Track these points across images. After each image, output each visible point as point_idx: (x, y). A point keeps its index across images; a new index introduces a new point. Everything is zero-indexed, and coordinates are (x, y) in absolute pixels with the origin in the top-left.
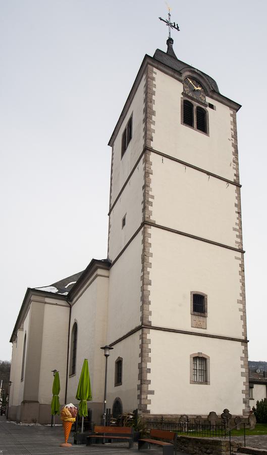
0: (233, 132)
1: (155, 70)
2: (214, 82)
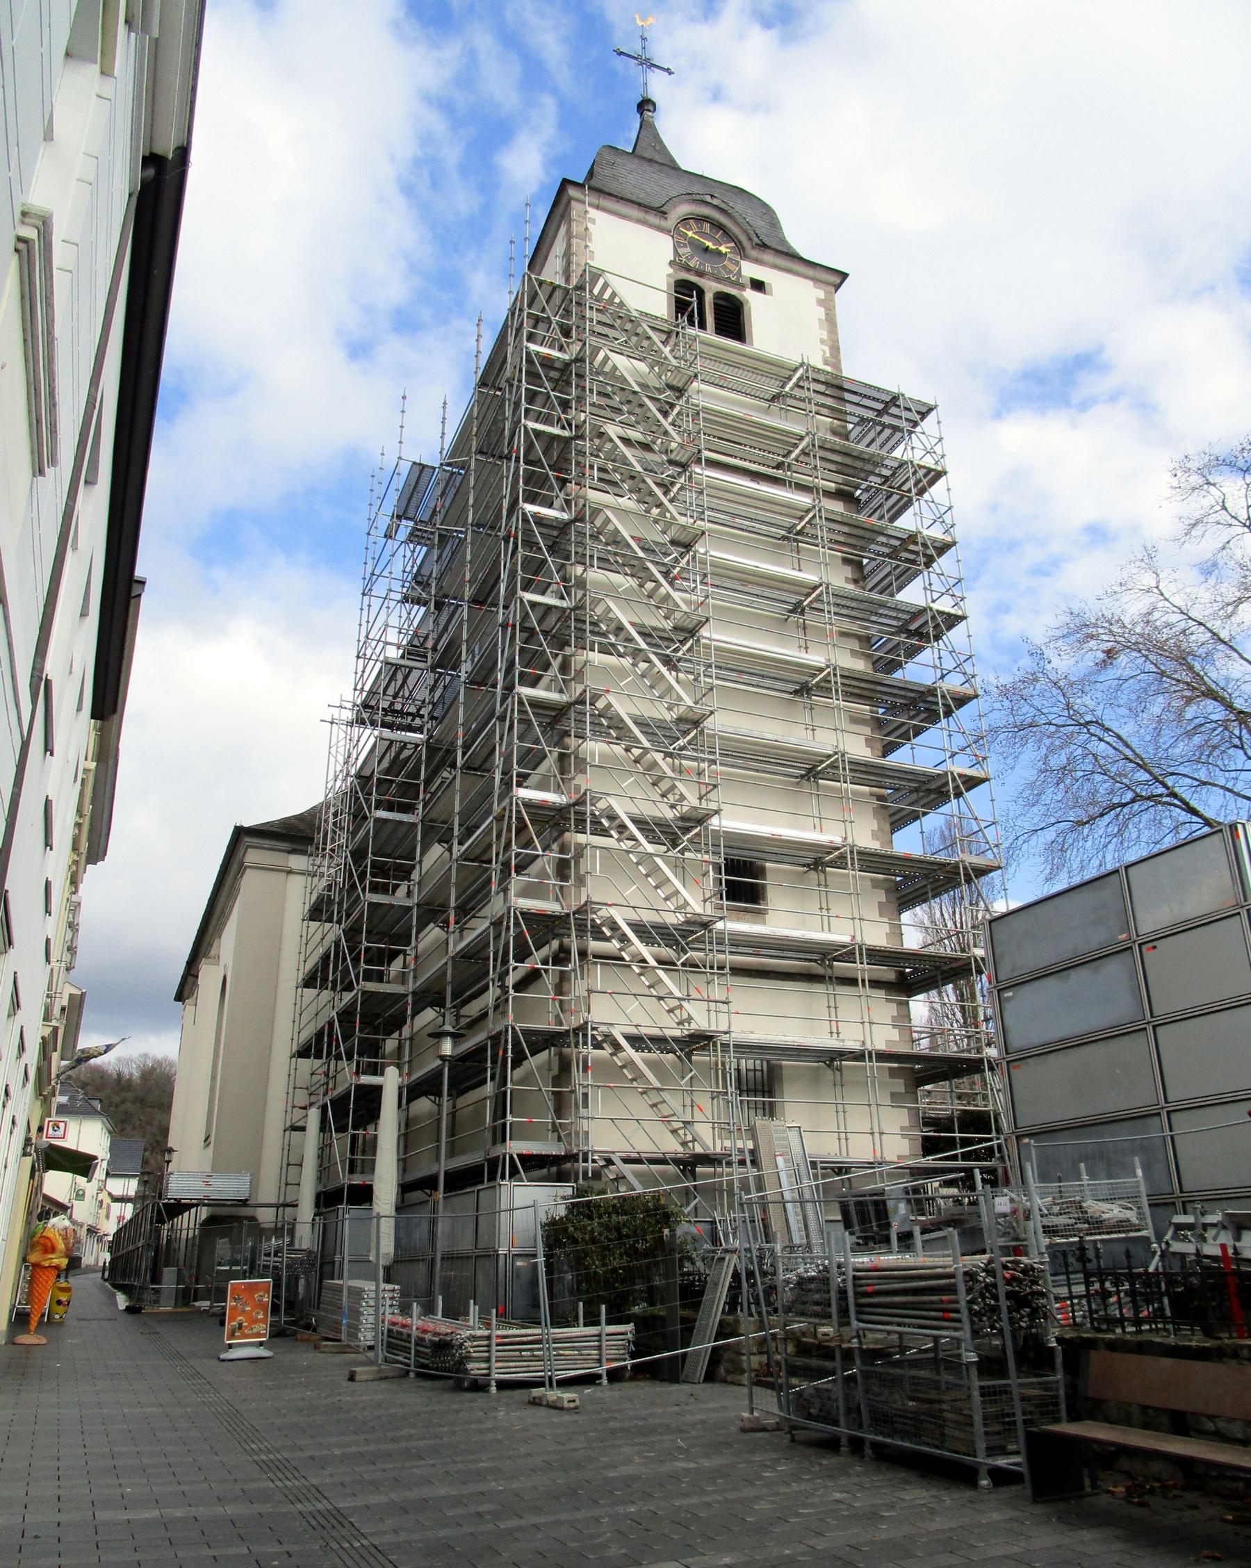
0: (827, 349)
1: (593, 213)
2: (767, 211)
